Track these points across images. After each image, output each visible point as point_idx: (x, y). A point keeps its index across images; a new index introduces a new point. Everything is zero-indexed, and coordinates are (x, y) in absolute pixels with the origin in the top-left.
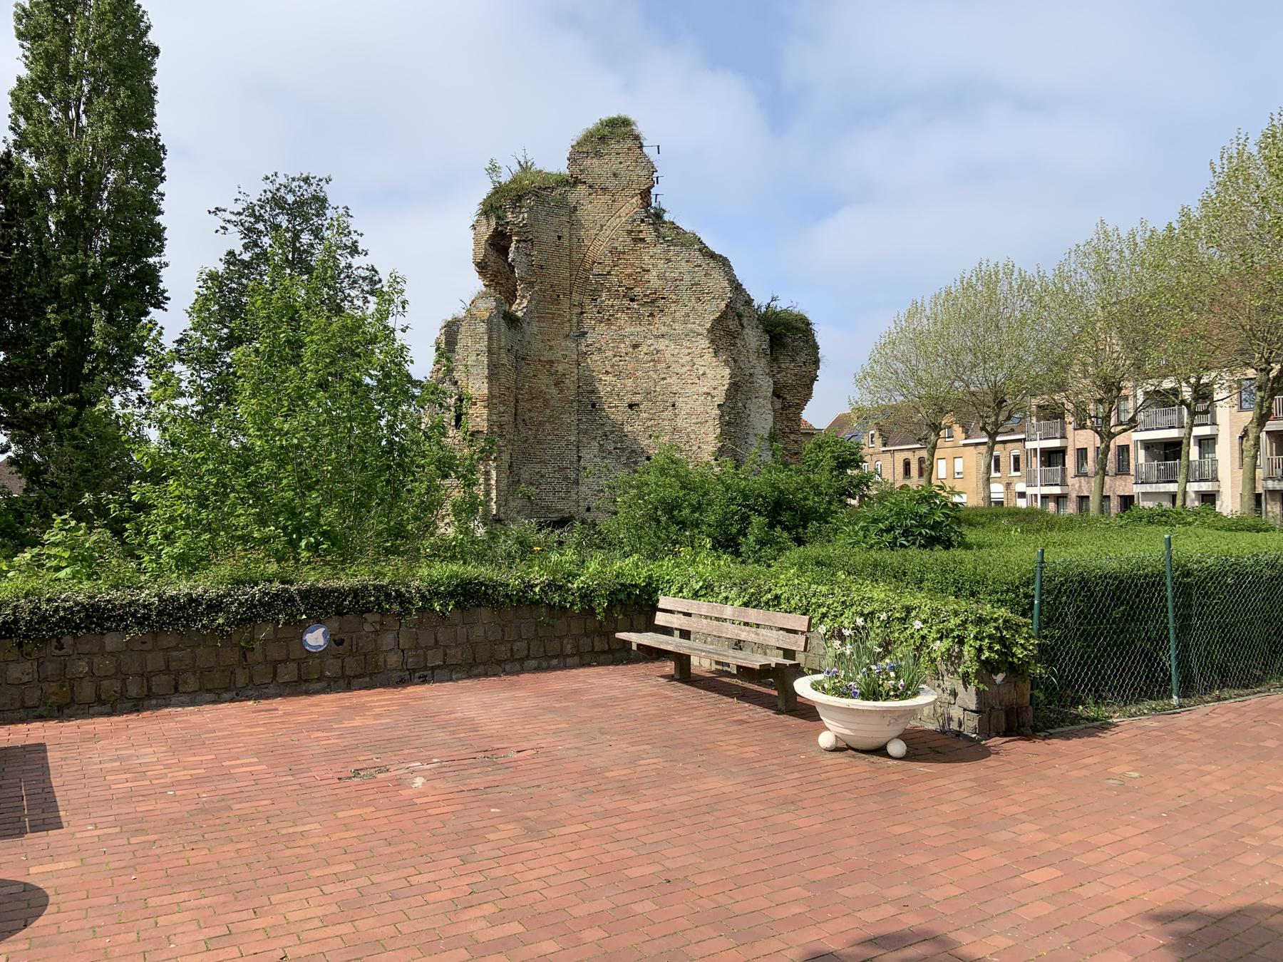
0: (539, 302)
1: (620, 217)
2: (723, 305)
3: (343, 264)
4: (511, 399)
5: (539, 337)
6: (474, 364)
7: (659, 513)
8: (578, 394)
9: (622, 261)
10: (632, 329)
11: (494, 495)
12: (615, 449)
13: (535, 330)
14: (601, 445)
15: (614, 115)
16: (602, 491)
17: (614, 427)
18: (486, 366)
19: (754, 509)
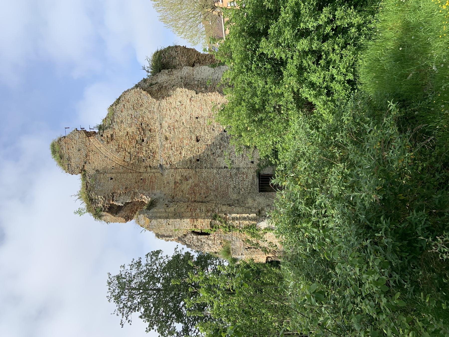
0: (144, 189)
1: (100, 148)
2: (144, 93)
3: (145, 268)
4: (193, 205)
5: (162, 189)
6: (174, 226)
7: (256, 119)
8: (192, 168)
9: (123, 146)
10: (158, 140)
11: (245, 215)
12: (220, 149)
13: (159, 191)
14: (218, 156)
15: (50, 152)
16: (242, 155)
17: (209, 149)
18: (175, 220)
19: (254, 51)
